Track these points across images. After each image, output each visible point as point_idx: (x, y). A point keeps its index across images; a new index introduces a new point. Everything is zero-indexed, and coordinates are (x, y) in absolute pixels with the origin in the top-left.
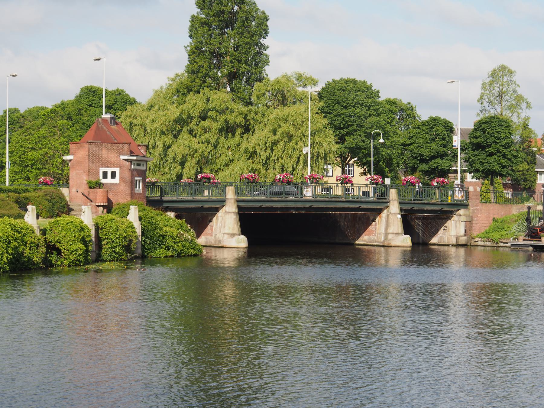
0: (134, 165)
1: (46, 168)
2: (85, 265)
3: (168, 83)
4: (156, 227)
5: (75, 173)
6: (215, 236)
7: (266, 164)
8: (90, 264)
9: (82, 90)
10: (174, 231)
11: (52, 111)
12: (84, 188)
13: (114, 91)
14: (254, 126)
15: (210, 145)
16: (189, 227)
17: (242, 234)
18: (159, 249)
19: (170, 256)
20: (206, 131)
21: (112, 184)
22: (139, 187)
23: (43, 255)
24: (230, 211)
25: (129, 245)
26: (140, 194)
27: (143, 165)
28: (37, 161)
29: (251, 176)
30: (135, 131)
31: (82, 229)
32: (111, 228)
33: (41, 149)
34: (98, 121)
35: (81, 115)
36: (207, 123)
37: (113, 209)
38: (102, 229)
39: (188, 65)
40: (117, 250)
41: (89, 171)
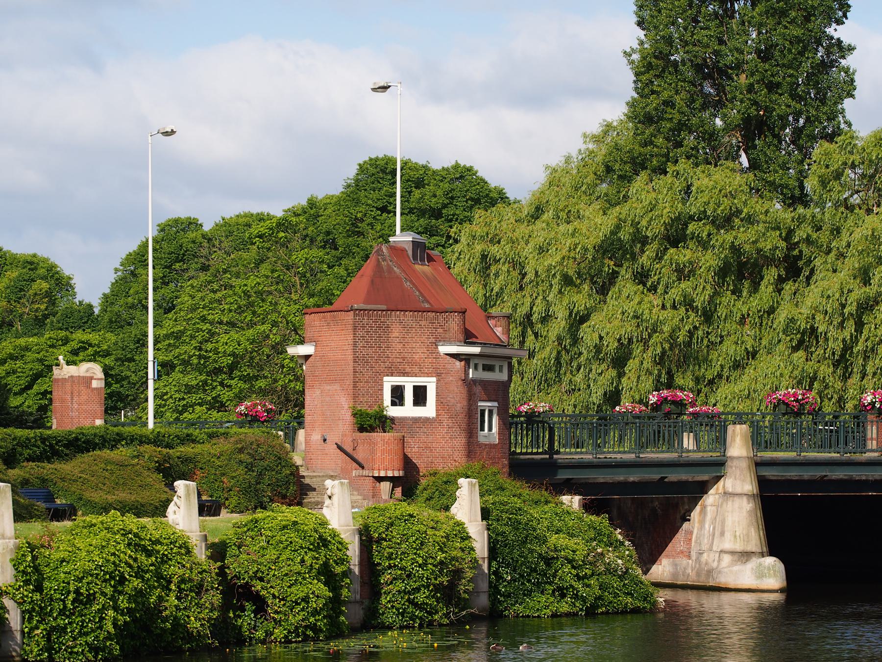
0: (476, 368)
1: (266, 377)
2: (328, 639)
3: (583, 147)
4: (527, 534)
5: (318, 392)
6: (698, 560)
7: (842, 362)
8: (348, 637)
9: (362, 168)
10: (578, 547)
11: (283, 224)
12: (343, 427)
13: (447, 170)
14: (810, 261)
15: (692, 315)
16: (618, 534)
17: (771, 553)
18: (536, 595)
19: (567, 615)
20: (683, 273)
21: (416, 420)
22: (490, 429)
23: (216, 614)
24: (739, 490)
25: (452, 586)
26: (492, 446)
27: (501, 367)
28: (242, 358)
29: (795, 395)
30: (497, 275)
31: (324, 542)
32: (405, 538)
33: (251, 325)
34: (379, 252)
35: (360, 234)
36: (683, 255)
37: (420, 488)
38: (379, 541)
39: (634, 99)
40: (420, 597)
41: (355, 387)
